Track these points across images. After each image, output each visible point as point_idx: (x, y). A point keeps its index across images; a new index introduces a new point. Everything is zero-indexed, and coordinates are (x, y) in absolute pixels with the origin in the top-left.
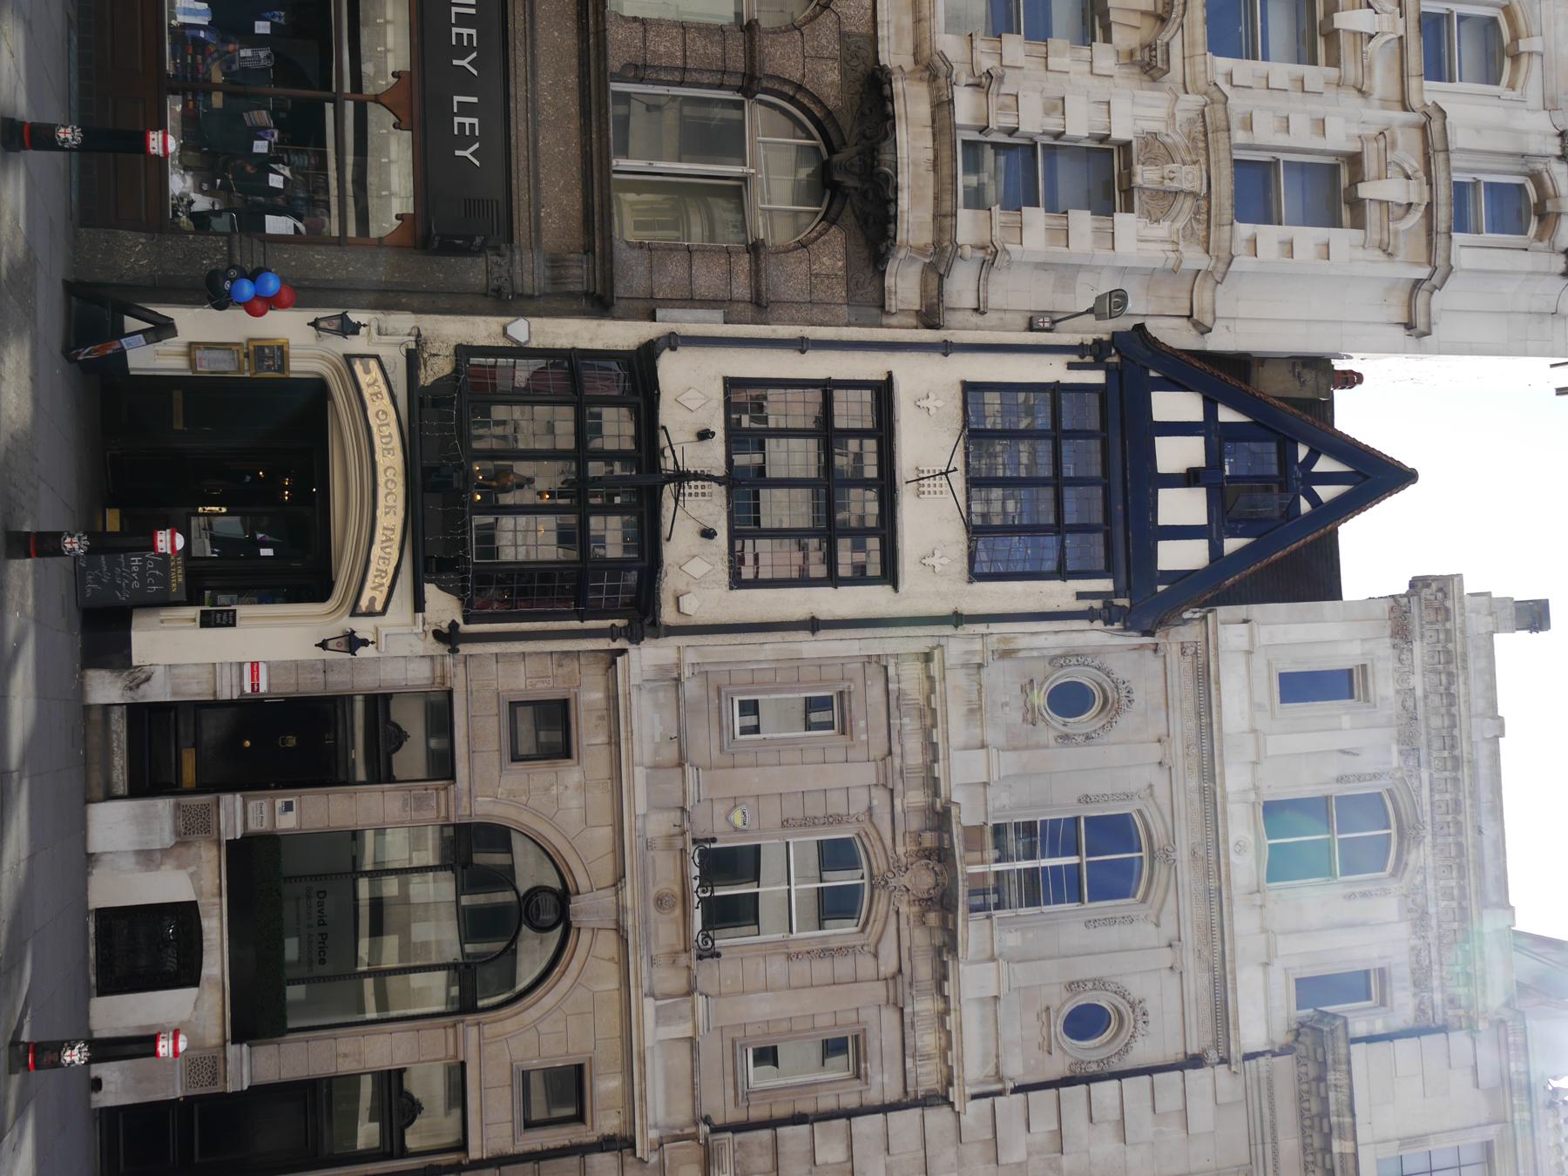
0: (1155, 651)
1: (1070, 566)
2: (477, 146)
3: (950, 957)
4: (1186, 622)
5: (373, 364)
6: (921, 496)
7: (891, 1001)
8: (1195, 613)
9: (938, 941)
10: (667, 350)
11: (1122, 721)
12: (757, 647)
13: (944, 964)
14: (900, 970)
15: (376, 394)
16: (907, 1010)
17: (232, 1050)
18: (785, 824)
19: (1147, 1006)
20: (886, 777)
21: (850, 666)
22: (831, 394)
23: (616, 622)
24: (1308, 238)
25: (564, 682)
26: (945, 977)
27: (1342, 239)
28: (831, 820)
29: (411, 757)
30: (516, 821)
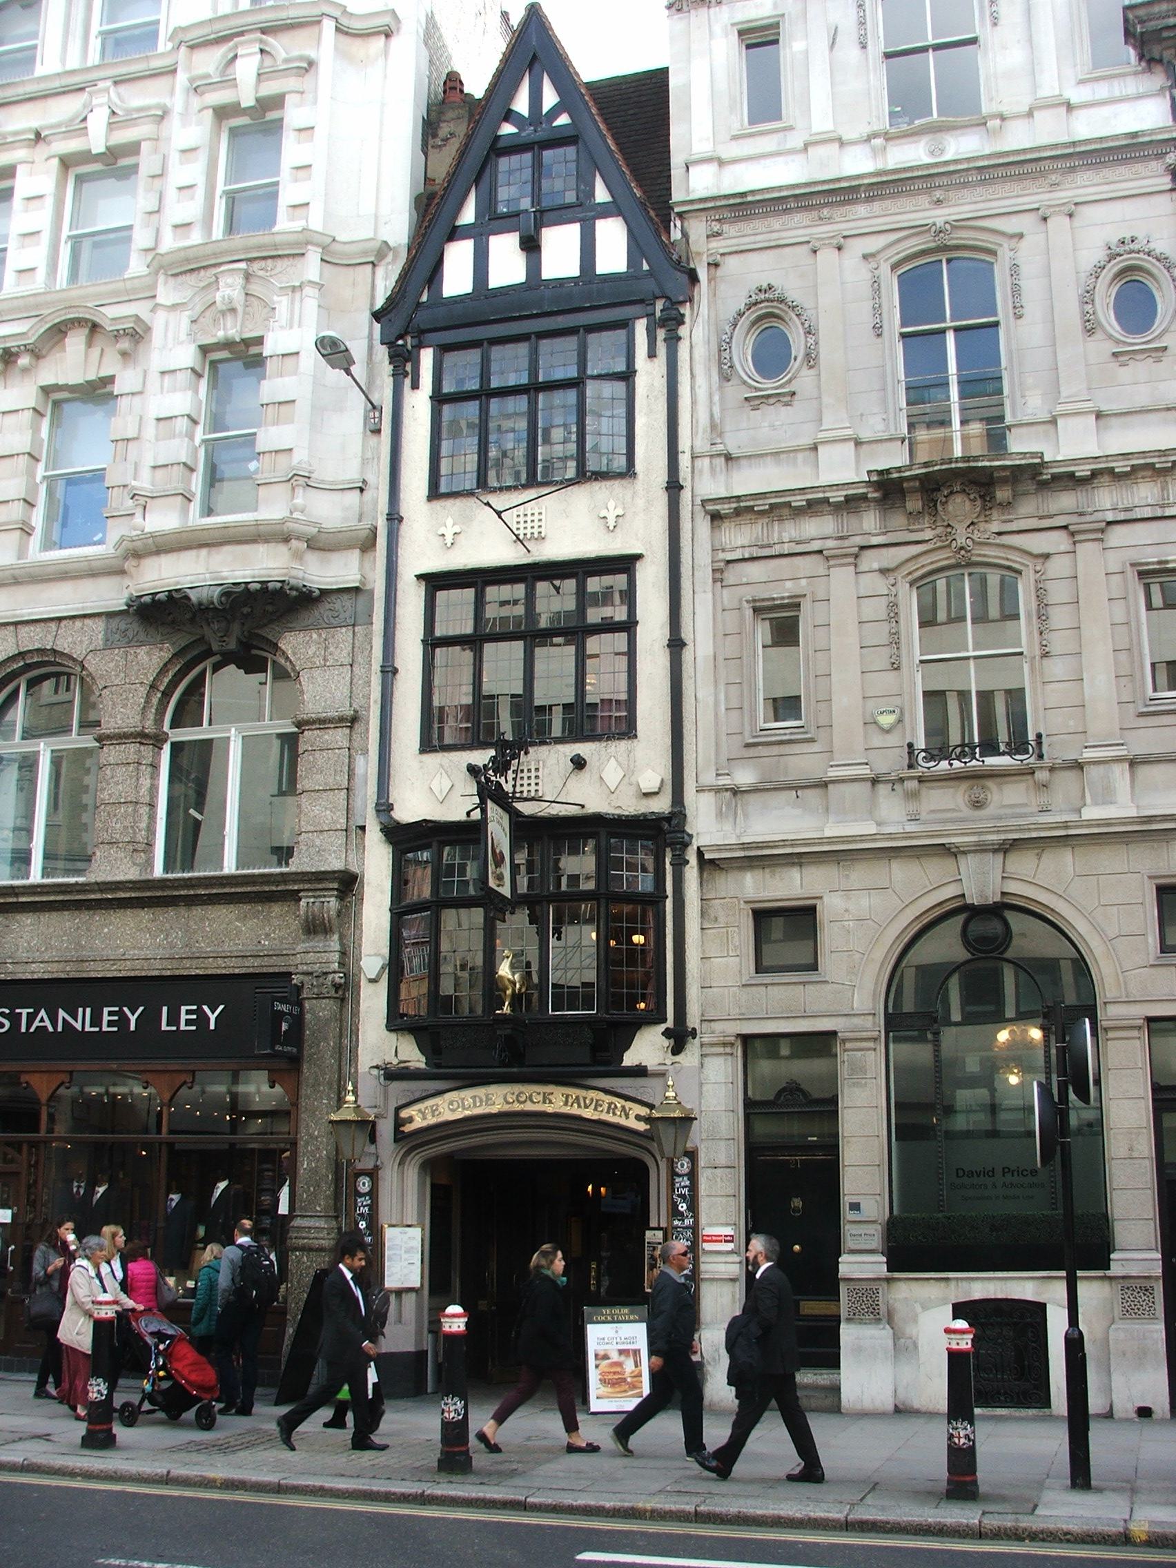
0: (716, 265)
1: (621, 367)
2: (205, 1008)
3: (1045, 471)
4: (685, 235)
5: (404, 1114)
6: (543, 535)
7: (1100, 536)
8: (675, 226)
9: (1032, 487)
10: (392, 813)
11: (793, 295)
12: (700, 706)
13: (1056, 478)
14: (1065, 527)
15: (433, 1112)
16: (1110, 517)
17: (1116, 1269)
18: (895, 667)
19: (1114, 241)
20: (846, 556)
21: (726, 602)
22: (439, 638)
23: (668, 861)
24: (292, 150)
25: (734, 915)
26: (1071, 475)
27: (294, 115)
28: (892, 615)
29: (804, 1069)
30: (882, 964)
